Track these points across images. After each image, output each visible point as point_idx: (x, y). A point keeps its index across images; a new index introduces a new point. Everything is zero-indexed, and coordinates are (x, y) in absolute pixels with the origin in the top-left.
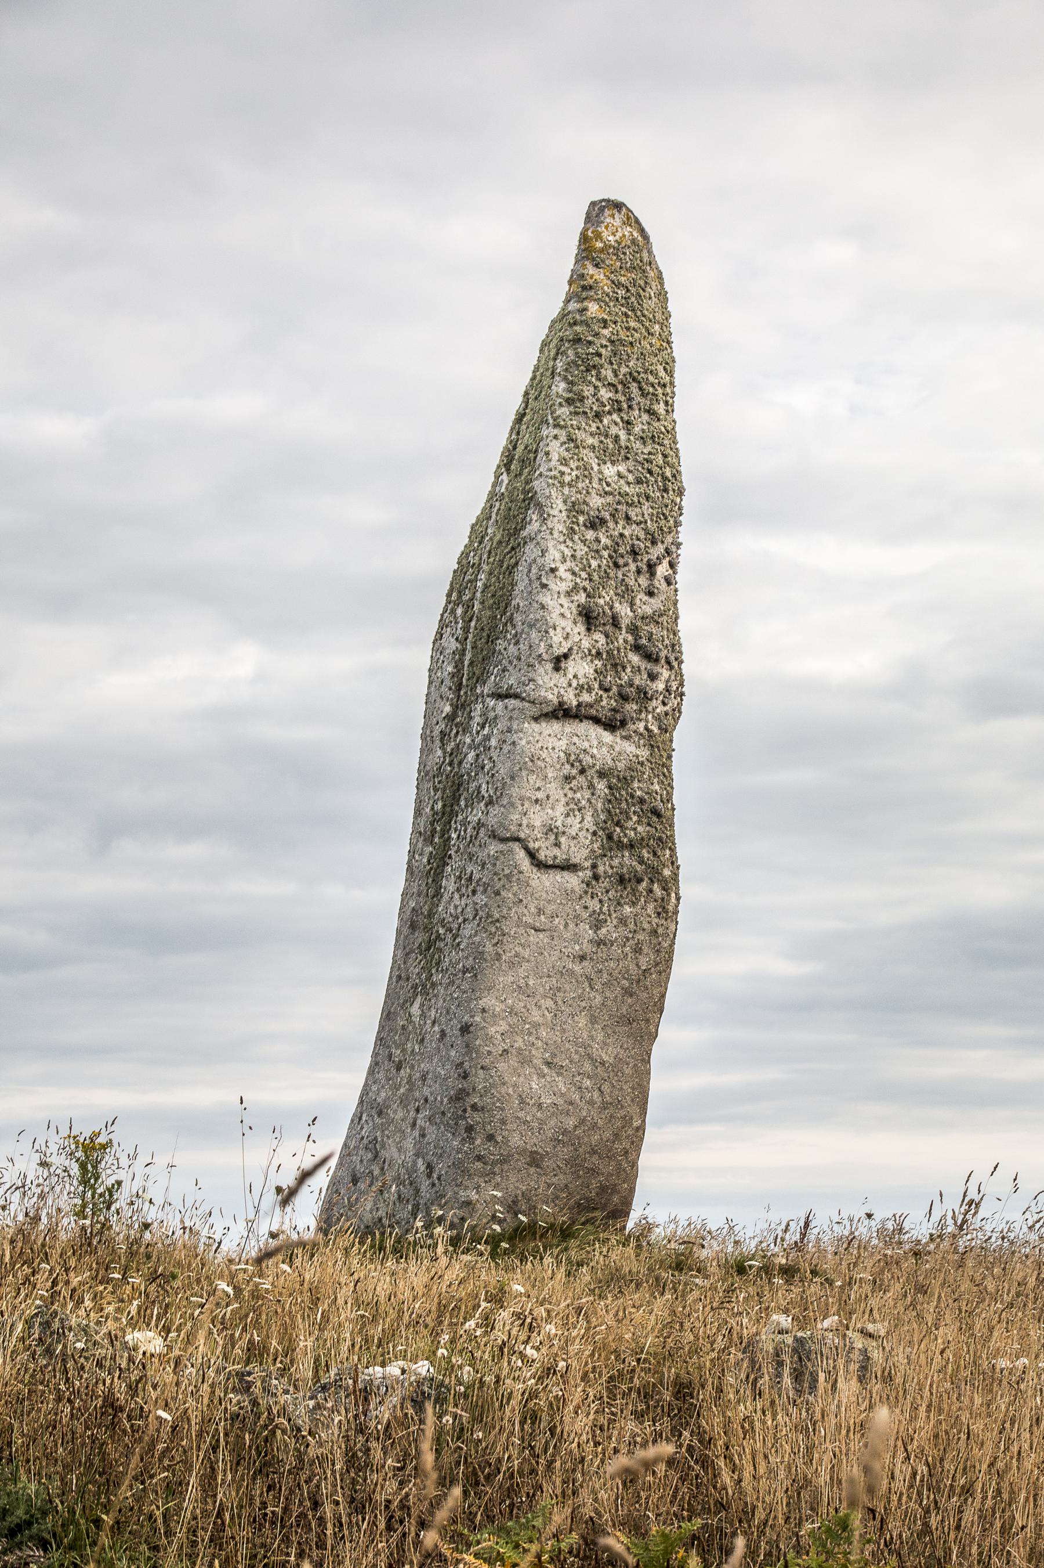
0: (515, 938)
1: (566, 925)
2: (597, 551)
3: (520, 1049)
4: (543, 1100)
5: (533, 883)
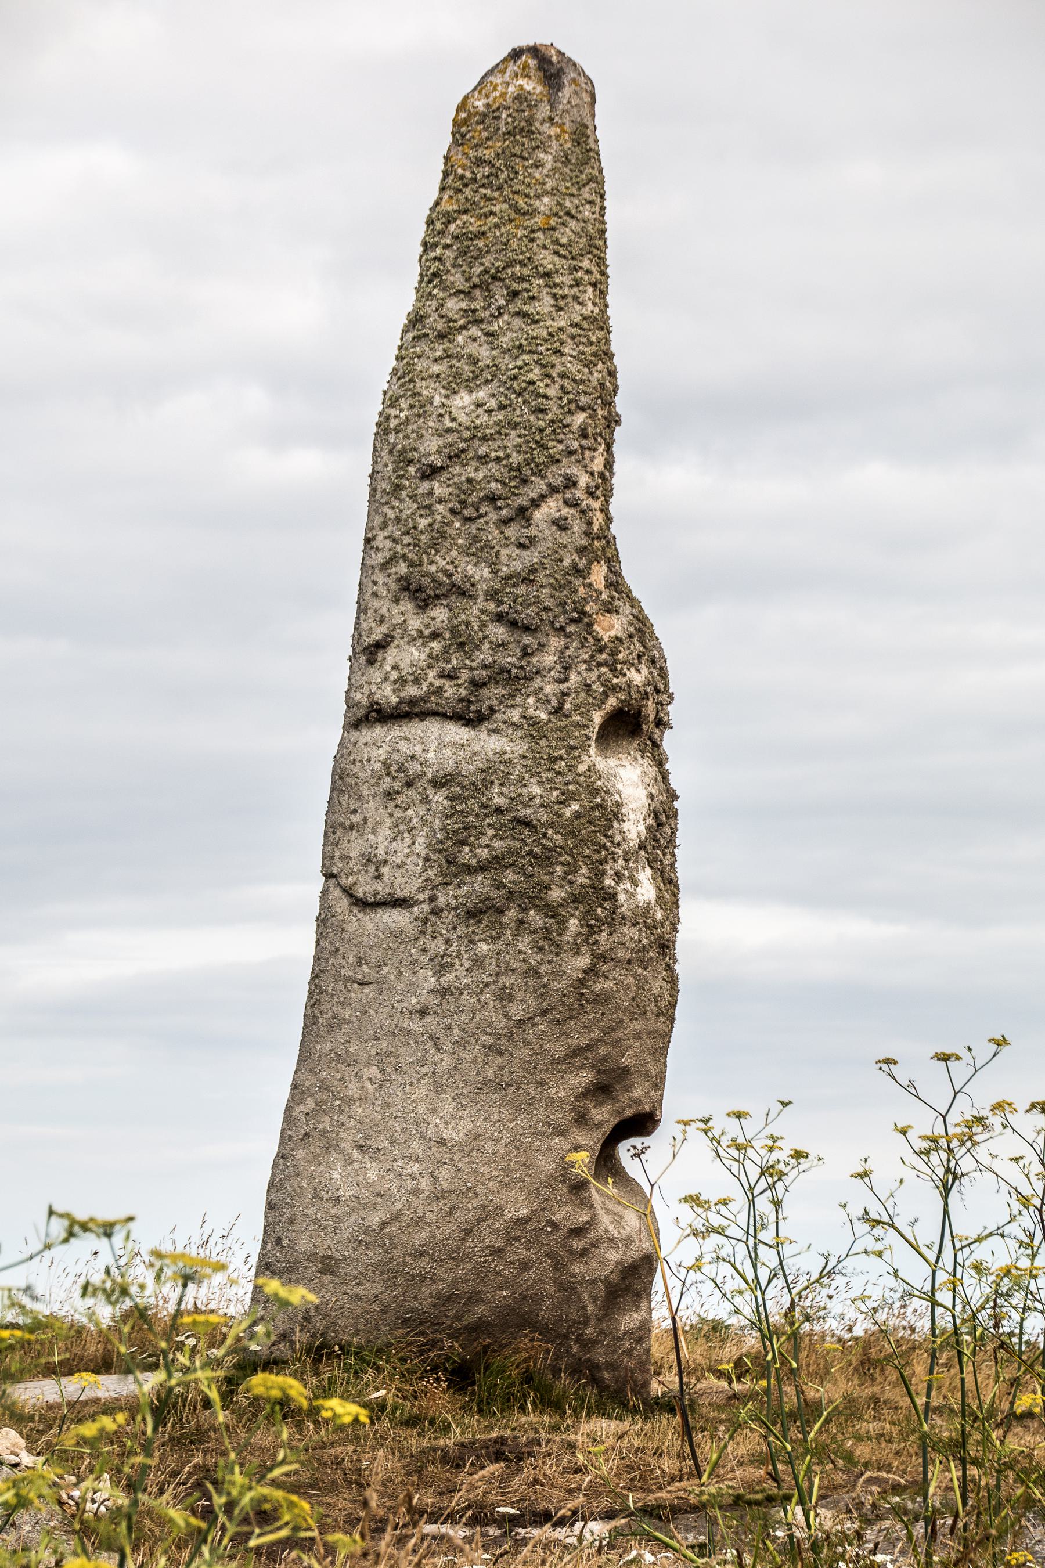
0: (332, 996)
1: (400, 974)
2: (428, 507)
3: (325, 1131)
4: (341, 1192)
5: (350, 928)
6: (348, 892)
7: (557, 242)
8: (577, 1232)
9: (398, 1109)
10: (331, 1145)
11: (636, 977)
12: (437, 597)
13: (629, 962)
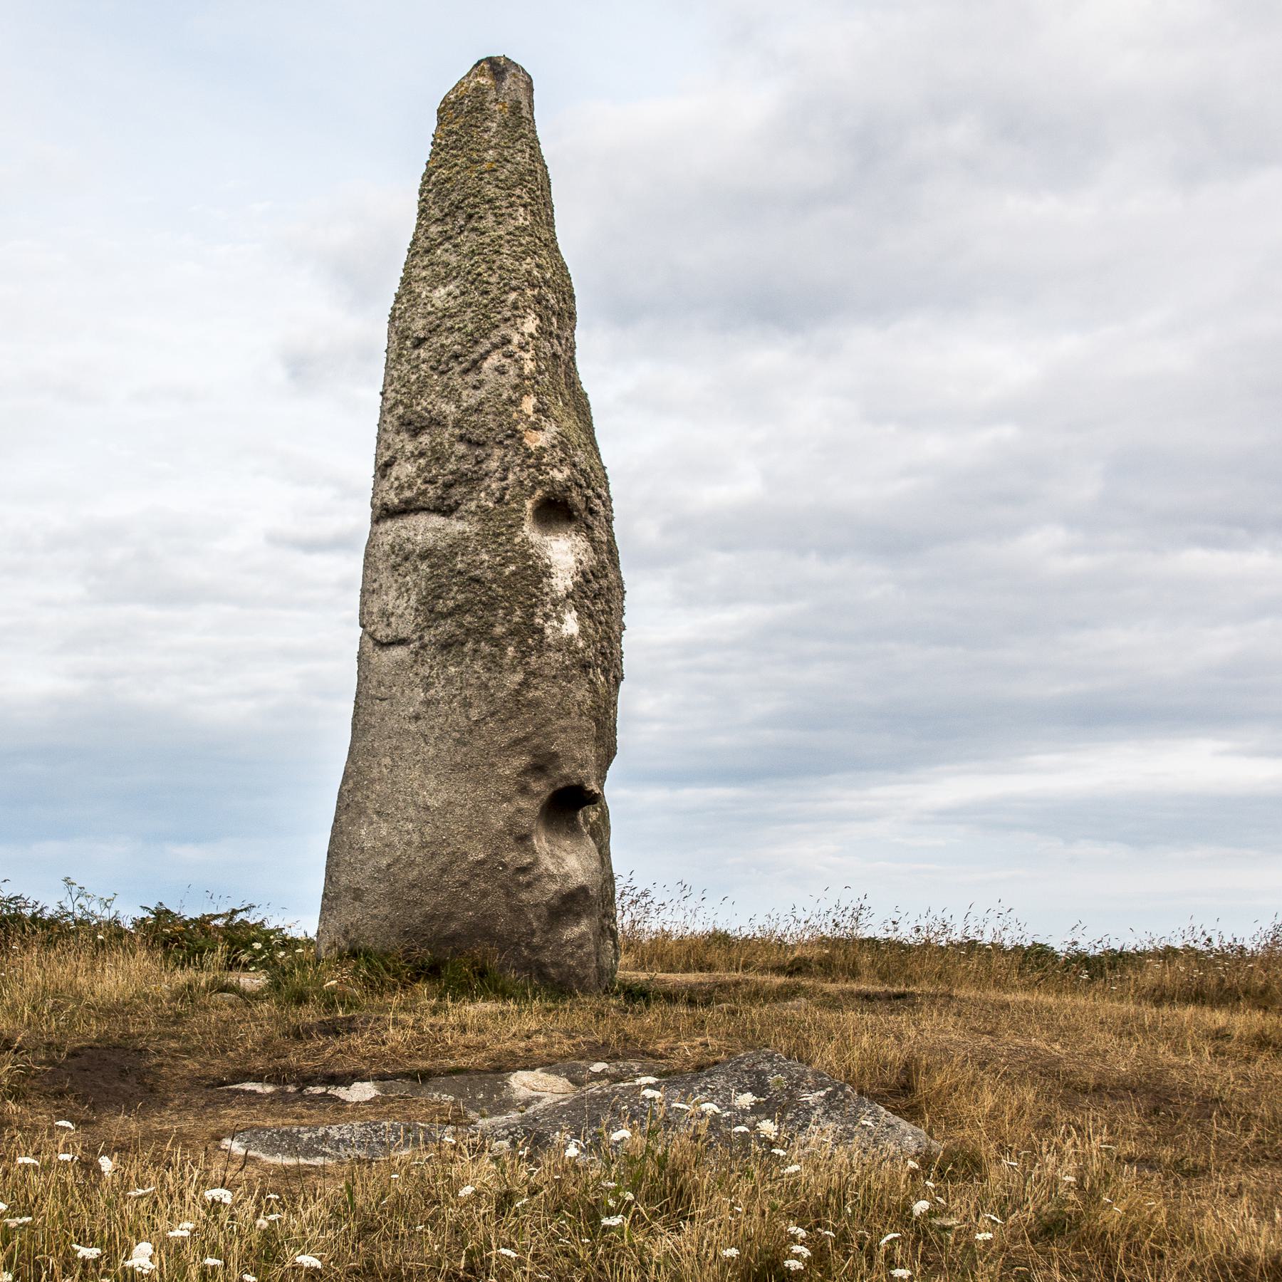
6: (372, 636)
7: (497, 179)
8: (523, 870)
9: (401, 786)
10: (362, 812)
11: (561, 688)
12: (423, 428)
13: (554, 677)
